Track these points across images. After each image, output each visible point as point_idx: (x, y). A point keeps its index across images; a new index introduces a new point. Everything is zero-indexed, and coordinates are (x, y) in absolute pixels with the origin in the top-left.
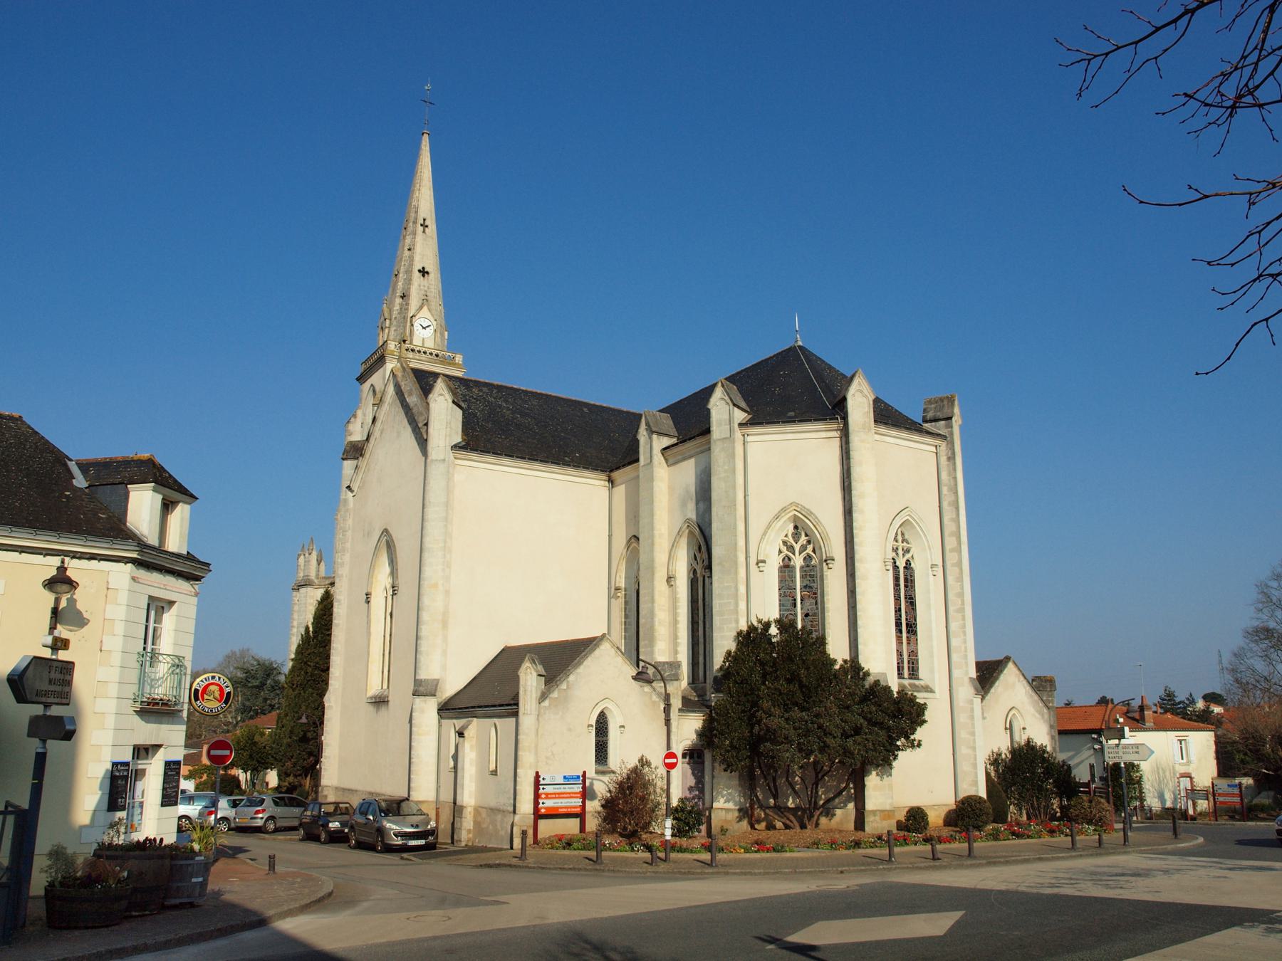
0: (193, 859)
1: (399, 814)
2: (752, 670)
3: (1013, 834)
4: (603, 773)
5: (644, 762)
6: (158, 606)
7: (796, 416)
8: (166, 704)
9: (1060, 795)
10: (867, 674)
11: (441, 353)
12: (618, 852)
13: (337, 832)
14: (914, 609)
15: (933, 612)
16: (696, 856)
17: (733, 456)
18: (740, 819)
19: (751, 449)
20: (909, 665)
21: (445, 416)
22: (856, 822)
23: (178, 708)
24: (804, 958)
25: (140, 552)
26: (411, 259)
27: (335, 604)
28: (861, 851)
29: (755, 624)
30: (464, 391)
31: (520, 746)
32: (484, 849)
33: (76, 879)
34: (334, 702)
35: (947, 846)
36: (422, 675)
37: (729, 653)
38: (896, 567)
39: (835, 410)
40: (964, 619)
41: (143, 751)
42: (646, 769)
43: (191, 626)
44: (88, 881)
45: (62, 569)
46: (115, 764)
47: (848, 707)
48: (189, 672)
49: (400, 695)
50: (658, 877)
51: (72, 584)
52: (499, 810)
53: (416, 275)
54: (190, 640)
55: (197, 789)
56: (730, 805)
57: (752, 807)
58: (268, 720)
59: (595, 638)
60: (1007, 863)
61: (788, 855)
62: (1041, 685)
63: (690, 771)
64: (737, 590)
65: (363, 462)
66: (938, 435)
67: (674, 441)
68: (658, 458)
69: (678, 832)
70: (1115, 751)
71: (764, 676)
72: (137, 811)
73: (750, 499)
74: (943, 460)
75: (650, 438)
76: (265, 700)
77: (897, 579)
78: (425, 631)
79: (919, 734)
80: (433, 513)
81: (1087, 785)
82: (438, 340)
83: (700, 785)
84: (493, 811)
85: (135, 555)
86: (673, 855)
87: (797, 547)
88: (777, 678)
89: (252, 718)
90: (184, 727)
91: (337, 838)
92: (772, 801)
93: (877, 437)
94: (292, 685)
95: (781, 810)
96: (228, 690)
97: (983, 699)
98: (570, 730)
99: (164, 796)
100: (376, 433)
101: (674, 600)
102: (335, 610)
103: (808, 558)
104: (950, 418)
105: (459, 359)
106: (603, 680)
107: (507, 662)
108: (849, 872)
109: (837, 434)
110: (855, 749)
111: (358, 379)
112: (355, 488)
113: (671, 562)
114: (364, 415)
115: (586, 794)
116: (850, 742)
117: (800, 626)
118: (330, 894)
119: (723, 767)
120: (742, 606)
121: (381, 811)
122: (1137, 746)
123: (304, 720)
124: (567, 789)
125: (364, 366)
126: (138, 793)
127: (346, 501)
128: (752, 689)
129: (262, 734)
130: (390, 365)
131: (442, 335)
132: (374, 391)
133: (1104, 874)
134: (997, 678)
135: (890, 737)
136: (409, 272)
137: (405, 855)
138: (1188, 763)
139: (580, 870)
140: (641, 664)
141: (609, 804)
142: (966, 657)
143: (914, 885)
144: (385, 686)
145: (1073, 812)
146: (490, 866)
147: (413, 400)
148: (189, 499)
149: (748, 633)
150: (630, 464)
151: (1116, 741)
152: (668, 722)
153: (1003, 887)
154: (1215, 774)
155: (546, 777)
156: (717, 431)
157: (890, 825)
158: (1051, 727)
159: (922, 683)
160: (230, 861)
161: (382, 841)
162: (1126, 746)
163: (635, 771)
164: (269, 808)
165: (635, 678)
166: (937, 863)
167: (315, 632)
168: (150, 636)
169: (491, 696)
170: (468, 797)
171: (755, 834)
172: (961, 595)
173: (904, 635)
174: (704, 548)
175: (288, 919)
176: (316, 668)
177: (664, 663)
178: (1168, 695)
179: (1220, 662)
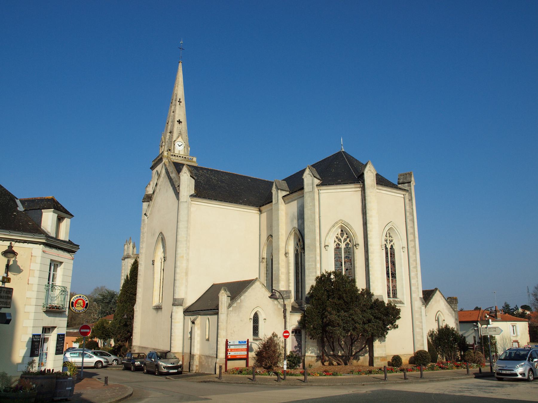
0: (67, 379)
1: (166, 358)
2: (323, 294)
3: (440, 367)
4: (257, 340)
5: (274, 335)
6: (55, 264)
8: (58, 308)
9: (460, 350)
10: (373, 295)
11: (187, 157)
12: (263, 375)
13: (138, 366)
14: (395, 267)
15: (403, 268)
16: (298, 377)
17: (314, 199)
18: (317, 361)
19: (322, 196)
20: (393, 292)
21: (187, 183)
22: (369, 362)
23: (64, 310)
25: (47, 240)
26: (174, 116)
27: (139, 265)
29: (325, 273)
30: (195, 172)
31: (219, 328)
32: (203, 374)
33: (11, 388)
34: (138, 308)
35: (411, 373)
36: (177, 297)
37: (312, 286)
38: (386, 248)
39: (359, 179)
40: (417, 271)
41: (47, 330)
42: (275, 338)
43: (70, 273)
44: (16, 389)
45: (10, 247)
46: (34, 335)
47: (365, 311)
48: (69, 294)
50: (280, 387)
51: (15, 254)
52: (210, 357)
53: (176, 123)
54: (70, 279)
55: (80, 347)
56: (313, 354)
58: (108, 318)
59: (253, 280)
60: (438, 381)
61: (339, 377)
62: (451, 301)
63: (295, 339)
64: (316, 258)
65: (151, 203)
67: (288, 193)
68: (281, 200)
69: (290, 367)
70: (483, 330)
71: (328, 296)
72: (44, 357)
74: (407, 200)
76: (111, 308)
77: (387, 253)
78: (178, 277)
79: (398, 322)
80: (182, 225)
81: (473, 345)
82: (186, 151)
83: (299, 346)
84: (208, 357)
85: (44, 241)
86: (287, 377)
87: (342, 240)
88: (334, 298)
89: (105, 316)
90: (66, 319)
91: (138, 369)
92: (332, 353)
93: (378, 190)
94: (121, 302)
95: (335, 356)
96: (87, 302)
97: (426, 307)
98: (241, 321)
99: (57, 350)
100: (157, 191)
101: (288, 263)
102: (139, 268)
103: (347, 244)
106: (257, 298)
107: (213, 292)
108: (367, 385)
109: (360, 189)
110: (369, 329)
111: (151, 168)
112: (148, 214)
113: (286, 246)
115: (249, 349)
116: (366, 326)
118: (131, 395)
119: (310, 337)
120: (318, 265)
121: (158, 357)
122: (495, 328)
124: (240, 347)
126: (45, 348)
127: (144, 220)
129: (107, 323)
130: (165, 160)
131: (187, 149)
133: (483, 386)
134: (431, 298)
135: (384, 324)
136: (173, 122)
137: (168, 377)
138: (517, 336)
139: (245, 383)
140: (273, 291)
142: (418, 288)
144: (161, 302)
145: (467, 358)
146: (205, 382)
147: (173, 175)
148: (71, 216)
149: (321, 277)
150: (268, 203)
151: (486, 326)
152: (285, 317)
153: (437, 392)
154: (529, 341)
155: (231, 342)
156: (307, 187)
157: (384, 363)
158: (456, 319)
159: (398, 300)
160: (89, 379)
161: (158, 370)
162: (490, 328)
163: (271, 339)
165: (270, 297)
166: (407, 381)
168: (51, 278)
169: (206, 306)
170: (197, 351)
171: (324, 367)
173: (390, 278)
174: (301, 240)
176: (131, 293)
177: (284, 291)
178: (506, 306)
179: (528, 292)
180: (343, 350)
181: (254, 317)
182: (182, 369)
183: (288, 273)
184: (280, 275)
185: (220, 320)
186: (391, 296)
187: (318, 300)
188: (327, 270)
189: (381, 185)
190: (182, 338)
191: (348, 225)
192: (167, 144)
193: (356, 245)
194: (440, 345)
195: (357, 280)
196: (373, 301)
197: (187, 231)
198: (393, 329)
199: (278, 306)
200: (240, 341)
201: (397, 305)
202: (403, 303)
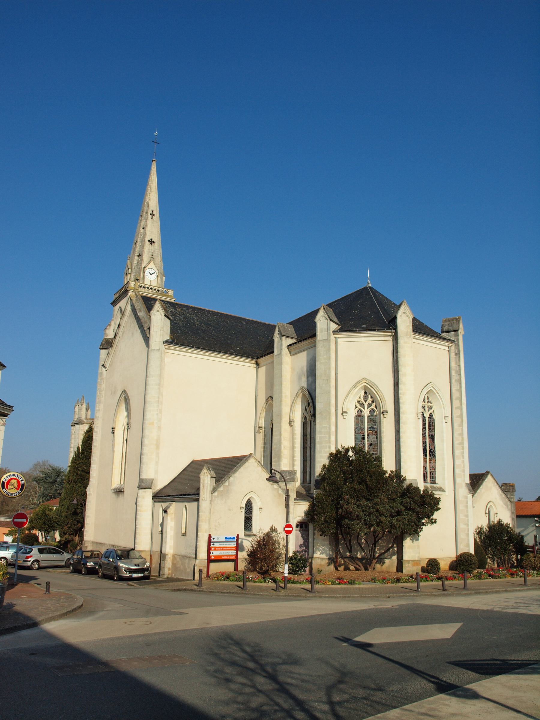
3: (490, 575)
5: (273, 530)
7: (367, 327)
11: (161, 289)
12: (257, 583)
14: (434, 442)
15: (445, 444)
16: (303, 586)
17: (329, 350)
19: (340, 346)
20: (430, 475)
21: (160, 323)
26: (144, 234)
29: (340, 449)
30: (173, 310)
31: (200, 519)
32: (178, 580)
34: (92, 491)
36: (144, 476)
37: (324, 466)
38: (424, 417)
39: (389, 324)
40: (463, 448)
47: (394, 499)
50: (279, 599)
53: (147, 243)
56: (324, 556)
59: (245, 456)
60: (486, 593)
61: (357, 586)
65: (112, 351)
66: (450, 340)
67: (295, 341)
68: (285, 350)
71: (345, 480)
74: (453, 355)
75: (281, 339)
77: (424, 424)
78: (145, 450)
82: (159, 281)
84: (184, 557)
86: (289, 585)
87: (366, 405)
88: (353, 481)
91: (91, 572)
92: (348, 554)
95: (353, 559)
96: (22, 482)
100: (120, 334)
104: (457, 330)
105: (171, 293)
106: (250, 480)
107: (194, 469)
108: (394, 597)
109: (390, 338)
111: (112, 304)
112: (107, 365)
113: (291, 411)
115: (239, 548)
116: (394, 520)
119: (320, 533)
120: (333, 438)
123: (75, 502)
125: (116, 296)
129: (51, 510)
131: (162, 278)
136: (143, 241)
137: (130, 583)
139: (233, 593)
141: (252, 554)
142: (464, 471)
144: (122, 483)
146: (179, 590)
147: (142, 314)
149: (336, 454)
150: (269, 354)
155: (215, 537)
156: (321, 335)
157: (417, 569)
159: (438, 486)
167: (83, 450)
172: (462, 434)
173: (428, 457)
174: (311, 404)
180: (364, 551)
181: (246, 505)
182: (150, 572)
183: (293, 448)
187: (332, 484)
188: (343, 445)
190: (150, 531)
191: (373, 385)
192: (134, 271)
193: (384, 412)
196: (405, 487)
197: (159, 389)
202: (444, 491)
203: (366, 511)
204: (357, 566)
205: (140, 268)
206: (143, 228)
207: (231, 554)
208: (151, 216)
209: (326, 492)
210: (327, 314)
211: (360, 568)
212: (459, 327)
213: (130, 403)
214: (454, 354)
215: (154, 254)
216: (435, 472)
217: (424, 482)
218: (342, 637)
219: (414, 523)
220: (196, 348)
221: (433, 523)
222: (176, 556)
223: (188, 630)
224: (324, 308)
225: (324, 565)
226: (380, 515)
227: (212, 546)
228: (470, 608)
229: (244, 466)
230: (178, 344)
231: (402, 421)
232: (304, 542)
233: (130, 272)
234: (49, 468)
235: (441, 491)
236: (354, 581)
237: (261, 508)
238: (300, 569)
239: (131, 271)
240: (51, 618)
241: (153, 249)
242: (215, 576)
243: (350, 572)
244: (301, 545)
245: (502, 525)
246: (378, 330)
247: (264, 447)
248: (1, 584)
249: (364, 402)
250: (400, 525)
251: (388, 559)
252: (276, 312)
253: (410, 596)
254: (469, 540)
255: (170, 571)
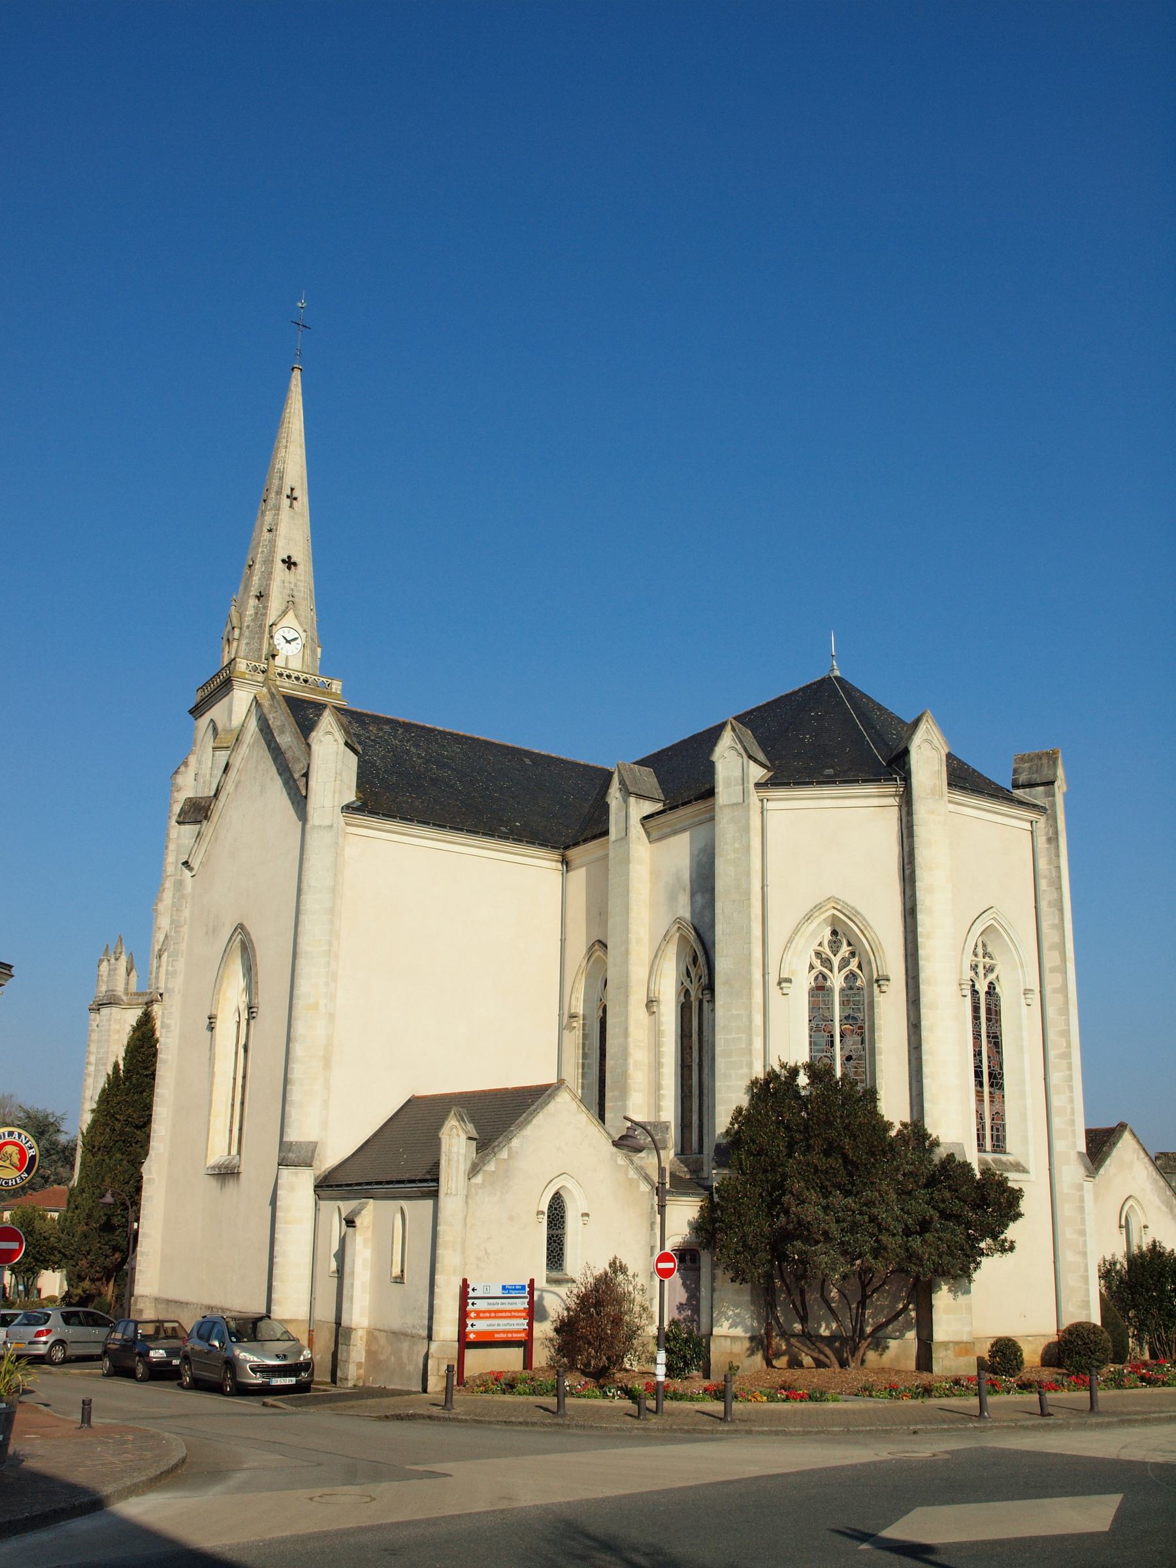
3: (1143, 1379)
4: (558, 1282)
5: (617, 1267)
7: (836, 775)
10: (936, 1144)
11: (311, 678)
12: (587, 1401)
14: (1000, 1053)
15: (1026, 1058)
16: (698, 1406)
17: (746, 829)
19: (773, 820)
20: (993, 1133)
21: (332, 763)
24: (921, 1565)
26: (273, 543)
28: (933, 1402)
29: (777, 1069)
30: (361, 729)
31: (440, 1241)
32: (383, 1393)
34: (157, 1172)
36: (292, 1136)
37: (739, 1111)
38: (975, 992)
39: (893, 767)
40: (1070, 1068)
47: (909, 1193)
49: (258, 1163)
50: (648, 1438)
52: (405, 1335)
53: (279, 567)
56: (739, 1331)
57: (768, 1334)
59: (546, 1088)
60: (1146, 1422)
61: (831, 1405)
64: (750, 1021)
65: (208, 828)
66: (1034, 807)
67: (659, 806)
68: (636, 830)
69: (672, 1370)
71: (791, 1147)
73: (770, 891)
74: (1041, 841)
75: (626, 802)
77: (976, 1009)
78: (297, 1071)
79: (1012, 1232)
82: (308, 659)
83: (693, 1302)
84: (397, 1335)
86: (667, 1404)
87: (836, 961)
88: (809, 1148)
91: (160, 1373)
92: (798, 1327)
93: (951, 807)
95: (809, 1338)
96: (31, 1153)
100: (229, 787)
104: (1052, 783)
105: (337, 686)
106: (562, 1147)
107: (418, 1121)
108: (927, 1432)
109: (894, 801)
111: (191, 712)
112: (195, 864)
113: (651, 979)
114: (200, 762)
115: (534, 1312)
116: (916, 1243)
117: (838, 1074)
118: (184, 1460)
119: (730, 1274)
120: (758, 1043)
123: (109, 1199)
124: (507, 1305)
125: (200, 693)
128: (773, 1165)
129: (43, 1218)
131: (314, 652)
132: (215, 729)
136: (268, 562)
137: (269, 1400)
139: (534, 1424)
141: (566, 1328)
142: (1072, 1122)
143: (1029, 1454)
144: (234, 1151)
146: (399, 1417)
147: (286, 739)
149: (767, 1082)
150: (594, 837)
155: (478, 1287)
156: (725, 793)
157: (966, 1366)
159: (1010, 1158)
164: (57, 1327)
167: (127, 1071)
169: (398, 1164)
170: (359, 1316)
172: (1066, 1033)
173: (986, 1089)
174: (701, 960)
175: (133, 1500)
180: (837, 1321)
181: (550, 1206)
182: (312, 1375)
183: (657, 1065)
184: (632, 1070)
185: (442, 1216)
186: (988, 1146)
187: (759, 1154)
188: (784, 1060)
189: (963, 788)
190: (308, 1273)
191: (854, 915)
192: (247, 634)
193: (881, 980)
194: (1135, 1307)
195: (882, 1094)
196: (936, 1161)
197: (331, 922)
198: (997, 1255)
199: (626, 1173)
200: (509, 1282)
201: (1011, 1175)
202: (1025, 1171)
203: (844, 1221)
204: (822, 1357)
205: (260, 626)
206: (270, 531)
207: (516, 1327)
208: (288, 502)
209: (744, 1174)
210: (741, 742)
211: (827, 1361)
212: (1055, 774)
213: (255, 956)
214: (1044, 838)
215: (295, 593)
216: (1004, 1126)
217: (979, 1151)
218: (854, 1530)
219: (962, 1250)
220: (419, 822)
221: (1006, 1250)
222: (377, 1333)
223: (469, 1514)
224: (733, 729)
225: (738, 1355)
226: (880, 1231)
227: (470, 1307)
228: (1122, 1457)
229: (545, 1110)
230: (378, 814)
231: (924, 1000)
232: (689, 1299)
233: (236, 636)
234: (22, 1115)
235: (1018, 1171)
236: (822, 1394)
237: (587, 1215)
238: (686, 1364)
239: (240, 634)
240: (128, 1488)
241: (293, 581)
242: (478, 1382)
243: (805, 1371)
244: (681, 1304)
245: (1161, 1255)
246: (864, 781)
247: (583, 1064)
248: (4, 1405)
249: (832, 956)
250: (930, 1254)
251: (895, 1339)
252: (606, 733)
253: (966, 1429)
254: (1087, 1290)
255: (362, 1371)
